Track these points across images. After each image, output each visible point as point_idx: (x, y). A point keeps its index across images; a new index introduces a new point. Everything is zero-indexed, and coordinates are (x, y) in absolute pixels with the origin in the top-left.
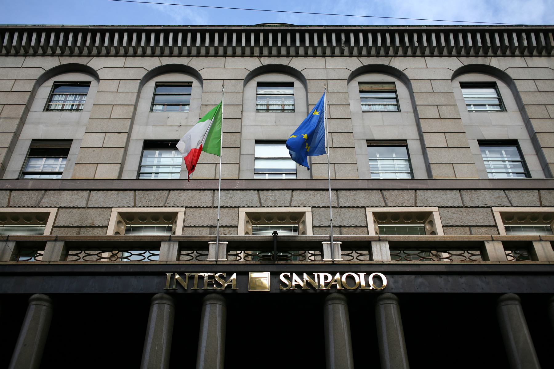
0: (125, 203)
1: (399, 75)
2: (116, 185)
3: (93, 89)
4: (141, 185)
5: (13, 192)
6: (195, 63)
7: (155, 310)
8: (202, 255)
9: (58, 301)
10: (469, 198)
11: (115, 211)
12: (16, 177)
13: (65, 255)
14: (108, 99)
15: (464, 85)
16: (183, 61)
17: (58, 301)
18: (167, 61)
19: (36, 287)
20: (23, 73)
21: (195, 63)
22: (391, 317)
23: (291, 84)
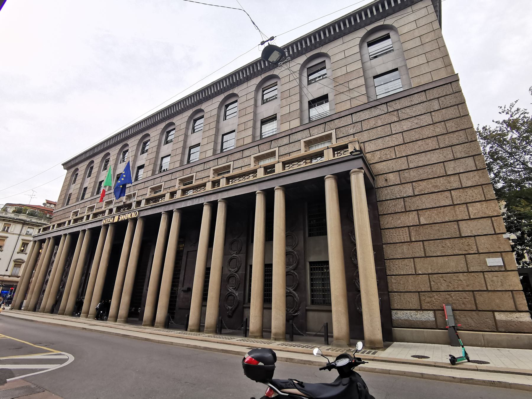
0: (305, 137)
1: (390, 27)
2: (368, 106)
3: (328, 64)
4: (312, 124)
5: (353, 115)
6: (388, 21)
7: (353, 178)
8: (345, 151)
9: (286, 189)
10: (431, 94)
11: (302, 141)
12: (251, 141)
13: (284, 168)
14: (286, 87)
15: (370, 44)
16: (231, 92)
17: (286, 189)
18: (369, 28)
19: (276, 184)
20: (351, 44)
21: (388, 21)
22: (279, 198)
23: (387, 37)
